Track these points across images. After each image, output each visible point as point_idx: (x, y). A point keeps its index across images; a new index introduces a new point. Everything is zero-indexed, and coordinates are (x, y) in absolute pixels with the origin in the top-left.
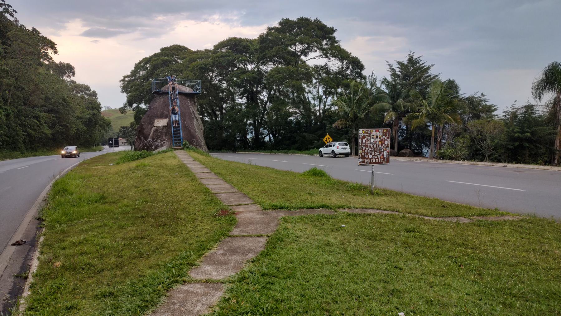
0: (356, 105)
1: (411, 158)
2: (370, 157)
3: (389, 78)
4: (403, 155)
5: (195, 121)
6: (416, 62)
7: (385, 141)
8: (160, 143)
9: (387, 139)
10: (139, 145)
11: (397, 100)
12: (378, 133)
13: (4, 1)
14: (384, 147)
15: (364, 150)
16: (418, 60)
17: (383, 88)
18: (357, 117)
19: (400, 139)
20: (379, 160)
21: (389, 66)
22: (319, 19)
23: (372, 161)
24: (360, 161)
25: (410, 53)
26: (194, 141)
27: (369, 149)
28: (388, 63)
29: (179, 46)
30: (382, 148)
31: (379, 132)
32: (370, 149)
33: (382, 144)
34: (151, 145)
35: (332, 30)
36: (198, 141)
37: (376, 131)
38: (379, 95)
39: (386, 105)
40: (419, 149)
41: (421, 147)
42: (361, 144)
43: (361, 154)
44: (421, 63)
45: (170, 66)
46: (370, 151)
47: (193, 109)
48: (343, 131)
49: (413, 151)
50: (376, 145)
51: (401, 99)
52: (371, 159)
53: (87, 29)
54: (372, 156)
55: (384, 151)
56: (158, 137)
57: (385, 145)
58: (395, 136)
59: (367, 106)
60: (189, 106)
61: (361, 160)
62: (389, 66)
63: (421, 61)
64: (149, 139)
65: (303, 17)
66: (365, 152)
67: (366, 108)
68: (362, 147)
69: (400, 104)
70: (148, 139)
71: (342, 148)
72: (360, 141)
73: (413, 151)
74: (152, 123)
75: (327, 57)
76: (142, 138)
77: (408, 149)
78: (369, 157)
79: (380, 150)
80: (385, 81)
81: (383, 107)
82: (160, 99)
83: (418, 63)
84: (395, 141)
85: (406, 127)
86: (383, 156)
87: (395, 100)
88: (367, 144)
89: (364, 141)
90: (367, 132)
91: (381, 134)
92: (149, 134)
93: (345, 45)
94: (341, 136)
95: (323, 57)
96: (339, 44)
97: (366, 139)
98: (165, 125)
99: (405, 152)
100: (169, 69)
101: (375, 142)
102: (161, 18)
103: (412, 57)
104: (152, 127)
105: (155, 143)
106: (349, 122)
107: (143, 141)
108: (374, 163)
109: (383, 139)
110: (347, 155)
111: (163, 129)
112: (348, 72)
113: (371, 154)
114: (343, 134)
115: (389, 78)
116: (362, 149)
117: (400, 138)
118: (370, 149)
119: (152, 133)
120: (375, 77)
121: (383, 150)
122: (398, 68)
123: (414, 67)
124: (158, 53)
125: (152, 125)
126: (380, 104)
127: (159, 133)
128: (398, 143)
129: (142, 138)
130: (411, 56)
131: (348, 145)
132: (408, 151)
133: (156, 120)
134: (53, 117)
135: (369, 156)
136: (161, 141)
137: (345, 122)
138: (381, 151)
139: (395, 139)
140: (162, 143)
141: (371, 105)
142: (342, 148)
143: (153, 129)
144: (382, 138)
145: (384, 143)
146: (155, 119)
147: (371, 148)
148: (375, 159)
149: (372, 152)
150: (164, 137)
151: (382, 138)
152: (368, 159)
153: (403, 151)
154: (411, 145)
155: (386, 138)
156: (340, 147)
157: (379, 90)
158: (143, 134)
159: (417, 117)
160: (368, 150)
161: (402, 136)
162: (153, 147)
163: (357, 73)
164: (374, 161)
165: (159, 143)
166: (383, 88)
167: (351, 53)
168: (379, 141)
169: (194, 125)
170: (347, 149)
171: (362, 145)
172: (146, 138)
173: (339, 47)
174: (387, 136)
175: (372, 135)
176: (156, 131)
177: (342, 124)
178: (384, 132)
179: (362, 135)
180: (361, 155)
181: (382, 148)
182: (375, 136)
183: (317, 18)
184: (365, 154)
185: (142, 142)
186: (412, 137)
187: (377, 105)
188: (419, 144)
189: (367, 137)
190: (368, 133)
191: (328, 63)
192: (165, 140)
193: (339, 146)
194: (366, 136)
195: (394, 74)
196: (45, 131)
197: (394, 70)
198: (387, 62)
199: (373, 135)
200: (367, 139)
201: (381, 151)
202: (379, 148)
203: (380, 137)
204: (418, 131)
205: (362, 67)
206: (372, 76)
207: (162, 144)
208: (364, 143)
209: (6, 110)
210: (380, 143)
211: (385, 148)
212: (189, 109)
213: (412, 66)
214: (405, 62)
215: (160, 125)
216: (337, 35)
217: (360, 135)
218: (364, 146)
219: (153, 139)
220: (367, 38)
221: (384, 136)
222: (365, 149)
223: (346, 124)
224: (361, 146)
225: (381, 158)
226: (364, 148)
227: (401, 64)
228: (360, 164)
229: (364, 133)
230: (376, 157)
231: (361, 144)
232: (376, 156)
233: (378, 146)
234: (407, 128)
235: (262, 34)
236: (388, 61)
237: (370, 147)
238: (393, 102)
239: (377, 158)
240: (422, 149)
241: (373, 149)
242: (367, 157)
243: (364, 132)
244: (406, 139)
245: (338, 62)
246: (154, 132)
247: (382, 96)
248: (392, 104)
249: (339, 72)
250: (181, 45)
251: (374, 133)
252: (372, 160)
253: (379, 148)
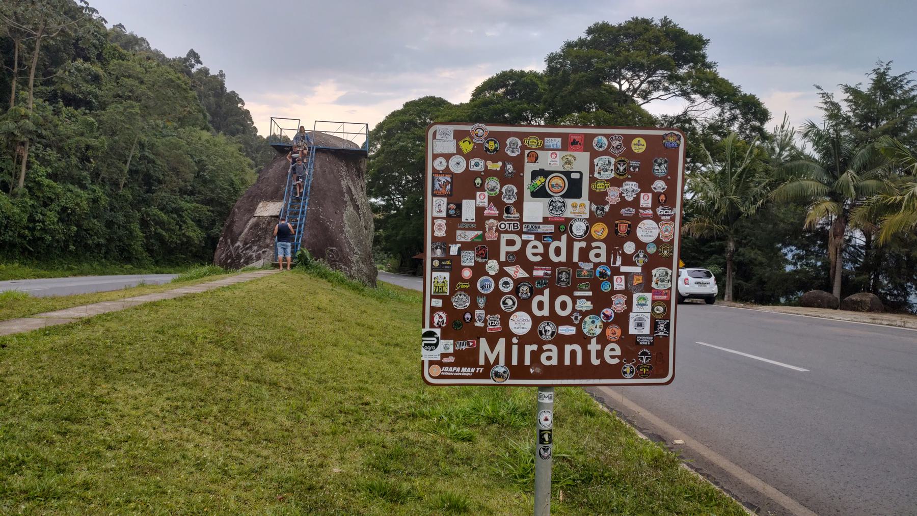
0: (737, 186)
1: (876, 315)
2: (520, 324)
3: (822, 124)
4: (855, 307)
5: (350, 209)
6: (895, 85)
7: (635, 220)
8: (257, 251)
9: (656, 202)
10: (220, 256)
11: (842, 173)
12: (581, 161)
13: (86, 3)
14: (628, 260)
15: (467, 274)
16: (901, 81)
17: (810, 150)
18: (740, 214)
19: (847, 268)
20: (586, 354)
21: (823, 97)
22: (670, 18)
23: (535, 356)
24: (436, 355)
25: (878, 66)
26: (332, 250)
27: (510, 270)
28: (819, 91)
29: (433, 98)
30: (616, 271)
31: (594, 154)
32: (522, 274)
33: (614, 243)
34: (239, 257)
35: (699, 42)
36: (341, 251)
37: (569, 143)
38: (796, 163)
39: (811, 185)
40: (899, 295)
41: (904, 289)
42: (441, 233)
43: (447, 301)
44: (906, 88)
45: (412, 130)
46: (518, 282)
47: (350, 183)
48: (711, 247)
49: (883, 298)
50: (563, 244)
51: (851, 171)
52: (524, 340)
53: (342, 93)
54: (536, 320)
55: (628, 293)
56: (257, 239)
57: (641, 245)
58: (833, 260)
59: (764, 188)
60: (342, 176)
61: (447, 346)
62: (823, 97)
63: (909, 82)
64: (238, 244)
65: (637, 18)
66: (473, 292)
67: (761, 193)
68: (454, 250)
69: (848, 181)
70: (236, 243)
71: (698, 283)
72: (436, 207)
73: (883, 298)
74: (251, 210)
75: (685, 94)
76: (229, 240)
77: (871, 292)
78: (512, 325)
79: (594, 283)
80: (812, 132)
81: (803, 189)
82: (281, 160)
83: (901, 87)
84: (835, 272)
85: (864, 239)
86: (625, 327)
87: (837, 173)
88: (491, 236)
89: (468, 212)
90: (491, 146)
91: (606, 169)
92: (240, 234)
93: (724, 72)
94: (707, 258)
95: (676, 95)
96: (715, 69)
97: (482, 199)
98: (274, 215)
99: (859, 299)
100: (410, 136)
101: (563, 227)
102: (447, 74)
103: (884, 74)
104: (250, 218)
105: (248, 251)
106: (717, 224)
107: (229, 246)
108: (549, 372)
109: (623, 203)
110: (709, 299)
111: (269, 223)
112: (735, 127)
113: (525, 306)
114: (712, 253)
115: (822, 124)
116: (453, 266)
117: (849, 267)
118: (522, 274)
119: (246, 230)
120: (790, 129)
121: (619, 283)
122: (846, 100)
123: (888, 97)
124: (398, 111)
125: (251, 213)
126: (795, 184)
127: (261, 230)
128: (842, 277)
129: (229, 240)
130: (882, 71)
131: (713, 277)
132: (868, 297)
133: (261, 205)
134: (208, 211)
135: (505, 318)
136: (260, 247)
137: (710, 223)
138: (606, 287)
139: (835, 267)
140: (261, 252)
141: (773, 186)
142: (698, 283)
143: (252, 221)
144: (613, 196)
145: (631, 235)
146: (260, 202)
147: (528, 266)
148: (560, 341)
149: (534, 292)
150: (268, 241)
151: (613, 196)
152: (501, 344)
153: (855, 297)
154: (877, 283)
155: (646, 201)
156: (692, 280)
157: (798, 156)
158: (232, 231)
159: (895, 208)
160: (502, 273)
161: (855, 262)
162: (242, 261)
163: (754, 129)
164: (550, 357)
165: (253, 252)
166: (810, 150)
167: (740, 86)
168: (592, 220)
169: (342, 217)
170: (708, 286)
171: (450, 238)
172: (234, 241)
173: (715, 75)
174: (660, 185)
175: (535, 175)
176: (256, 225)
177: (702, 228)
178: (630, 154)
179: (458, 166)
180: (447, 306)
181: (616, 271)
182: (558, 183)
183: (665, 17)
184: (474, 306)
185: (227, 250)
186: (879, 265)
187: (790, 187)
188: (898, 280)
189: (493, 183)
190: (498, 155)
191: (689, 109)
192: (268, 246)
193: (690, 278)
194: (488, 173)
195: (834, 112)
196: (187, 234)
197: (836, 106)
198: (818, 87)
199: (544, 173)
200: (496, 200)
201: (606, 287)
202: (587, 266)
203: (600, 187)
204: (895, 249)
205: (764, 116)
206: (783, 127)
207: (259, 254)
208: (469, 227)
209: (94, 191)
210: (600, 230)
211: (638, 270)
212: (340, 185)
213: (885, 97)
214: (865, 86)
215: (266, 214)
216: (711, 53)
217: (440, 165)
218: (465, 246)
219: (245, 243)
220: (794, 94)
221: (631, 187)
222: (479, 270)
223: (711, 229)
224: (444, 243)
225: (603, 340)
226: (468, 259)
227: (854, 92)
228: (436, 370)
229: (468, 157)
230: (567, 330)
231: (441, 233)
232: (567, 321)
233: (584, 255)
234: (868, 241)
235: (552, 53)
236: (820, 85)
237: (519, 258)
238: (831, 180)
239: (570, 340)
240: (908, 294)
241: (538, 273)
242: (494, 322)
243: (467, 147)
244: (864, 269)
245: (713, 106)
246: (251, 228)
247: (803, 165)
248: (829, 184)
249: (714, 128)
250: (436, 97)
251: (551, 160)
252: (529, 349)
253: (587, 266)
